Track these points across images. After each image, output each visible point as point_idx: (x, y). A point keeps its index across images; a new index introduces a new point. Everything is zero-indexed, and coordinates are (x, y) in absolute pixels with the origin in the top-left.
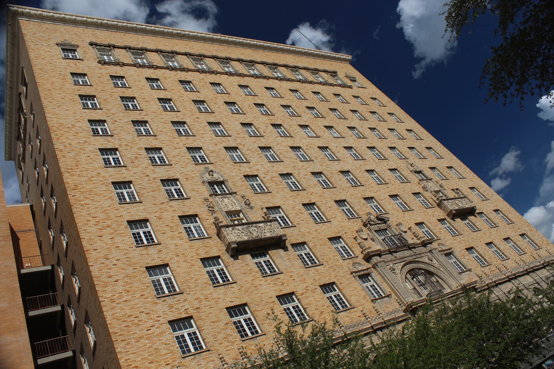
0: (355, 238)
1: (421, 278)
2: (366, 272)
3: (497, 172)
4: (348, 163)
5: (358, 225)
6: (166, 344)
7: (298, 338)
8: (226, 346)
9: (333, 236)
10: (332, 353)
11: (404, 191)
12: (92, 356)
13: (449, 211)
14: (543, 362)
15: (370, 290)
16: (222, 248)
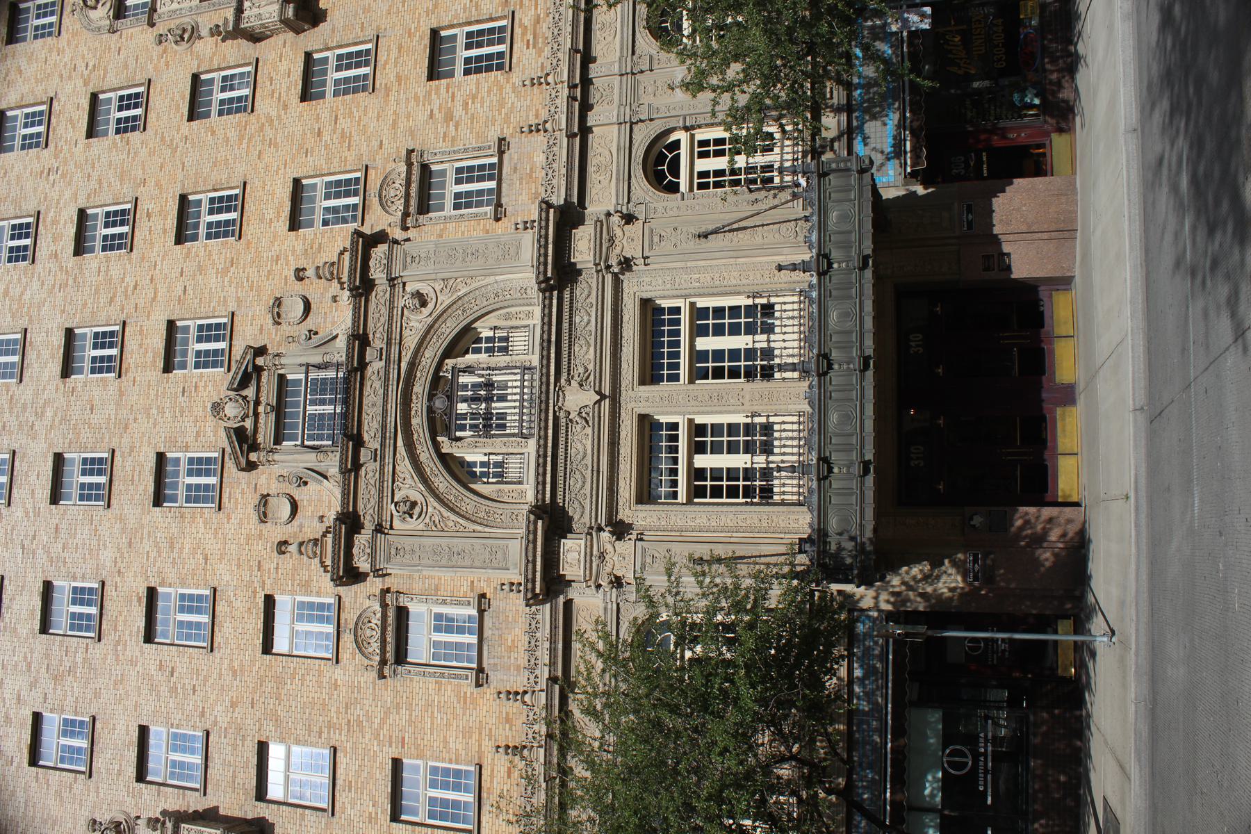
2: (391, 614)
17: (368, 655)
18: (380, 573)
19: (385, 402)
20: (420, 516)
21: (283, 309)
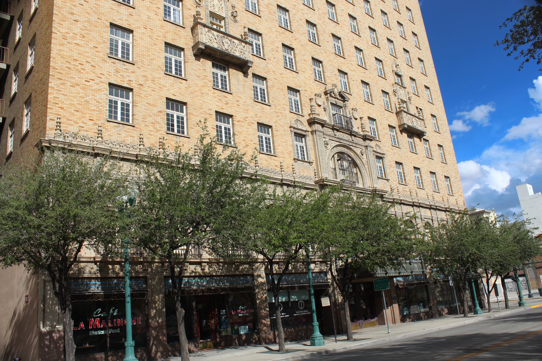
0: (310, 100)
1: (345, 164)
2: (303, 133)
3: (464, 115)
4: (344, 31)
5: (320, 89)
6: (98, 102)
7: (215, 155)
8: (150, 131)
9: (293, 87)
10: (237, 182)
11: (376, 84)
12: (24, 79)
13: (402, 123)
14: (396, 277)
15: (297, 149)
16: (189, 43)
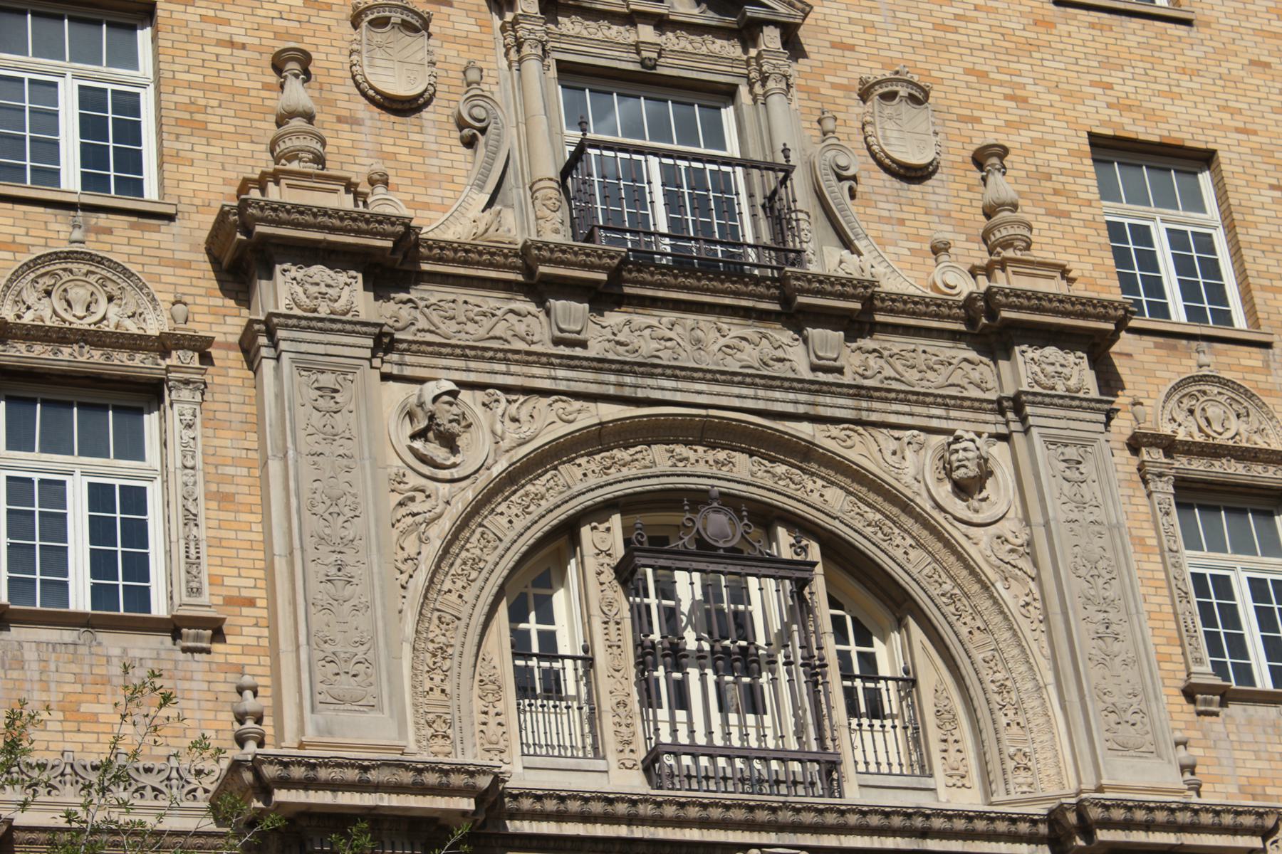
2: (139, 364)
17: (15, 287)
18: (263, 340)
19: (712, 376)
20: (423, 459)
21: (906, 109)
